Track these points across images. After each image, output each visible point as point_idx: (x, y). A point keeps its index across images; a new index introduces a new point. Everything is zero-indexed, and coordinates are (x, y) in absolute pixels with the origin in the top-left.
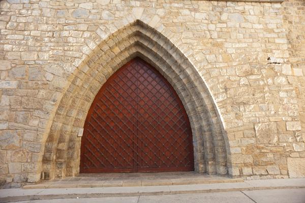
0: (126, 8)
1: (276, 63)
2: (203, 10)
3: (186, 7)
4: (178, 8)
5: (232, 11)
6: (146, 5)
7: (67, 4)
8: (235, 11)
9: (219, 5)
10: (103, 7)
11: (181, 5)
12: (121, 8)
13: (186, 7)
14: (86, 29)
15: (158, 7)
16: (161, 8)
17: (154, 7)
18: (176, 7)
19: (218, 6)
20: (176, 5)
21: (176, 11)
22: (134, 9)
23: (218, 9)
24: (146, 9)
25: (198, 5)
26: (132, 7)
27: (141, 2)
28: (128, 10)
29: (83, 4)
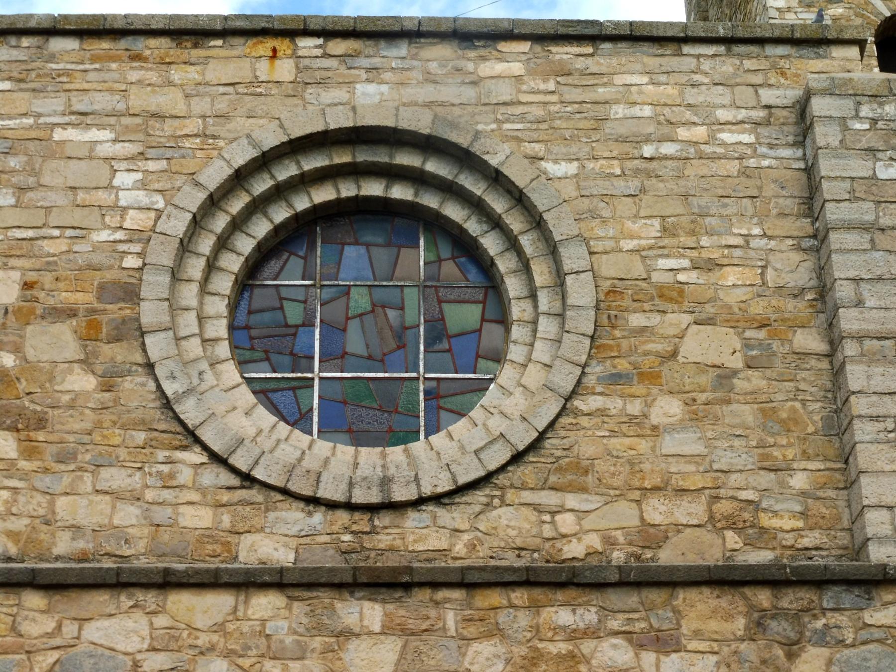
0: (317, 643)
1: (886, 309)
2: (697, 634)
3: (614, 624)
4: (574, 635)
5: (849, 637)
6: (412, 624)
7: (27, 628)
8: (864, 634)
9: (784, 603)
10: (203, 640)
11: (589, 616)
12: (289, 640)
13: (614, 624)
14: (300, 329)
15: (471, 630)
16: (489, 635)
17: (452, 632)
18: (564, 628)
19: (777, 613)
20: (564, 617)
21: (563, 647)
22: (353, 644)
23: (778, 627)
24: (414, 642)
25: (676, 611)
26: (346, 634)
27: (390, 607)
28: (327, 650)
29: (106, 623)
